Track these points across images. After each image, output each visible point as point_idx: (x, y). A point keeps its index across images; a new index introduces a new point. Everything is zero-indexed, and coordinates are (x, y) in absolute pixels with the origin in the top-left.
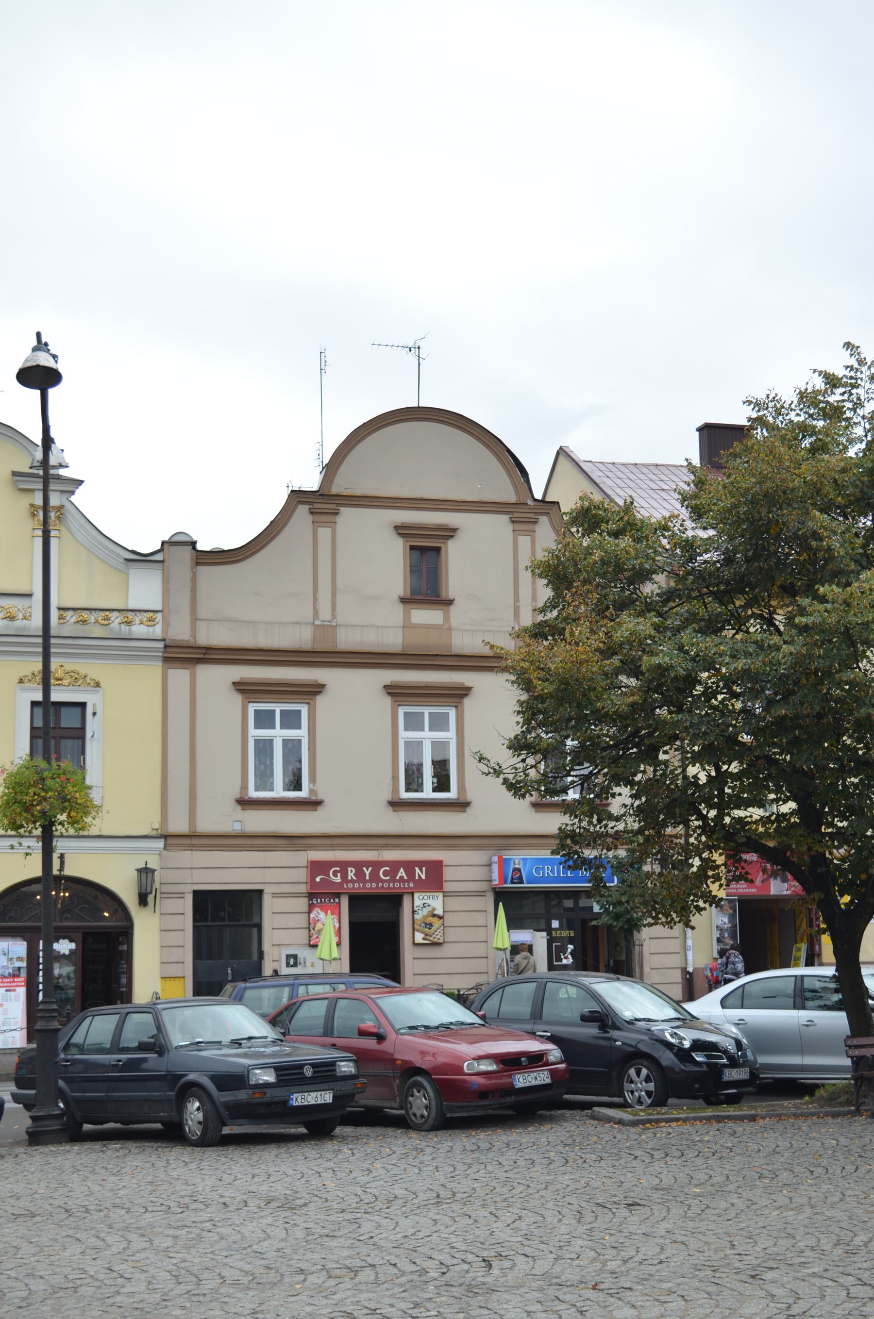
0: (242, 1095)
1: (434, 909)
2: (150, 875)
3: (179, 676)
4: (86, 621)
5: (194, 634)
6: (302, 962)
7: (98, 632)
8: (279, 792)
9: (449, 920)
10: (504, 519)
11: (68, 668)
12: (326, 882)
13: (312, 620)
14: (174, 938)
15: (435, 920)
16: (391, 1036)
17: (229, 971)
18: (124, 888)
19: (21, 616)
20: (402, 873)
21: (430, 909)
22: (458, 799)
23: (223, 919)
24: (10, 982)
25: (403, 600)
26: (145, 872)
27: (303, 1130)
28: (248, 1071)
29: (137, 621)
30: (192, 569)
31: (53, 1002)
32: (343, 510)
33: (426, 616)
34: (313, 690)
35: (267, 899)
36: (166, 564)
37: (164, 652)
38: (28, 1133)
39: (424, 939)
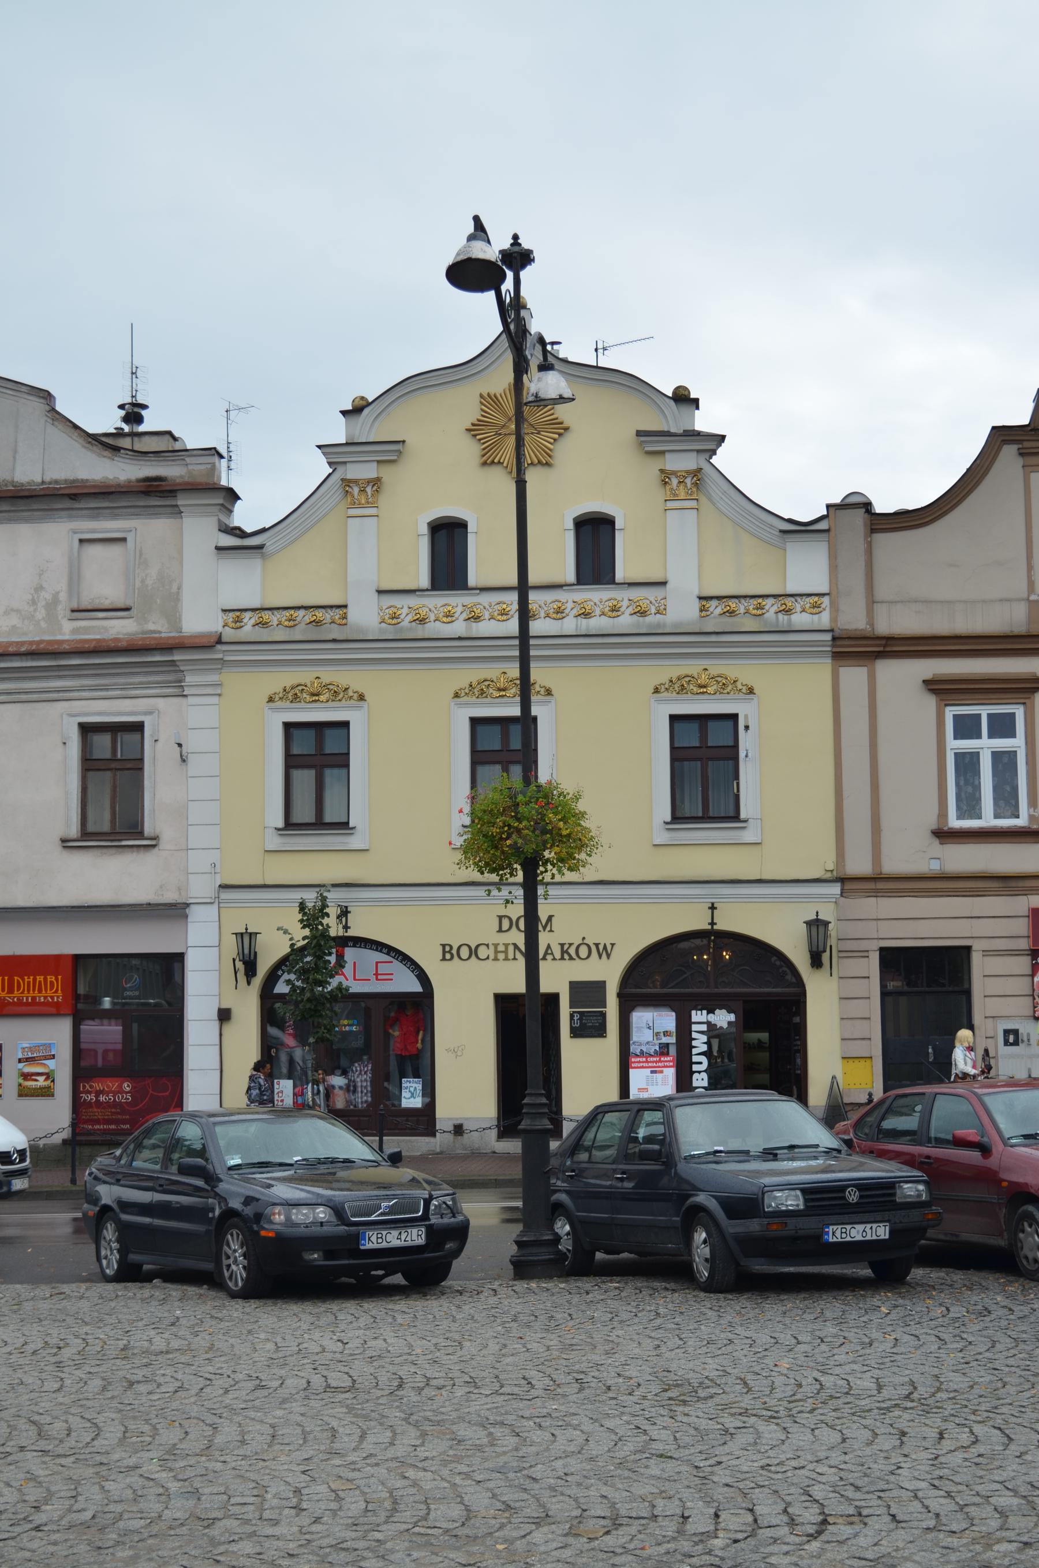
0: (754, 1226)
2: (821, 929)
3: (854, 675)
4: (734, 611)
5: (871, 621)
6: (1025, 1039)
7: (750, 624)
8: (988, 820)
11: (714, 671)
13: (1025, 595)
14: (857, 1009)
16: (998, 1148)
17: (930, 1050)
18: (793, 945)
19: (653, 611)
23: (944, 985)
24: (656, 1062)
26: (817, 926)
27: (867, 1272)
28: (763, 1194)
30: (866, 538)
31: (541, 1095)
35: (976, 958)
36: (832, 533)
37: (833, 646)
38: (512, 1262)
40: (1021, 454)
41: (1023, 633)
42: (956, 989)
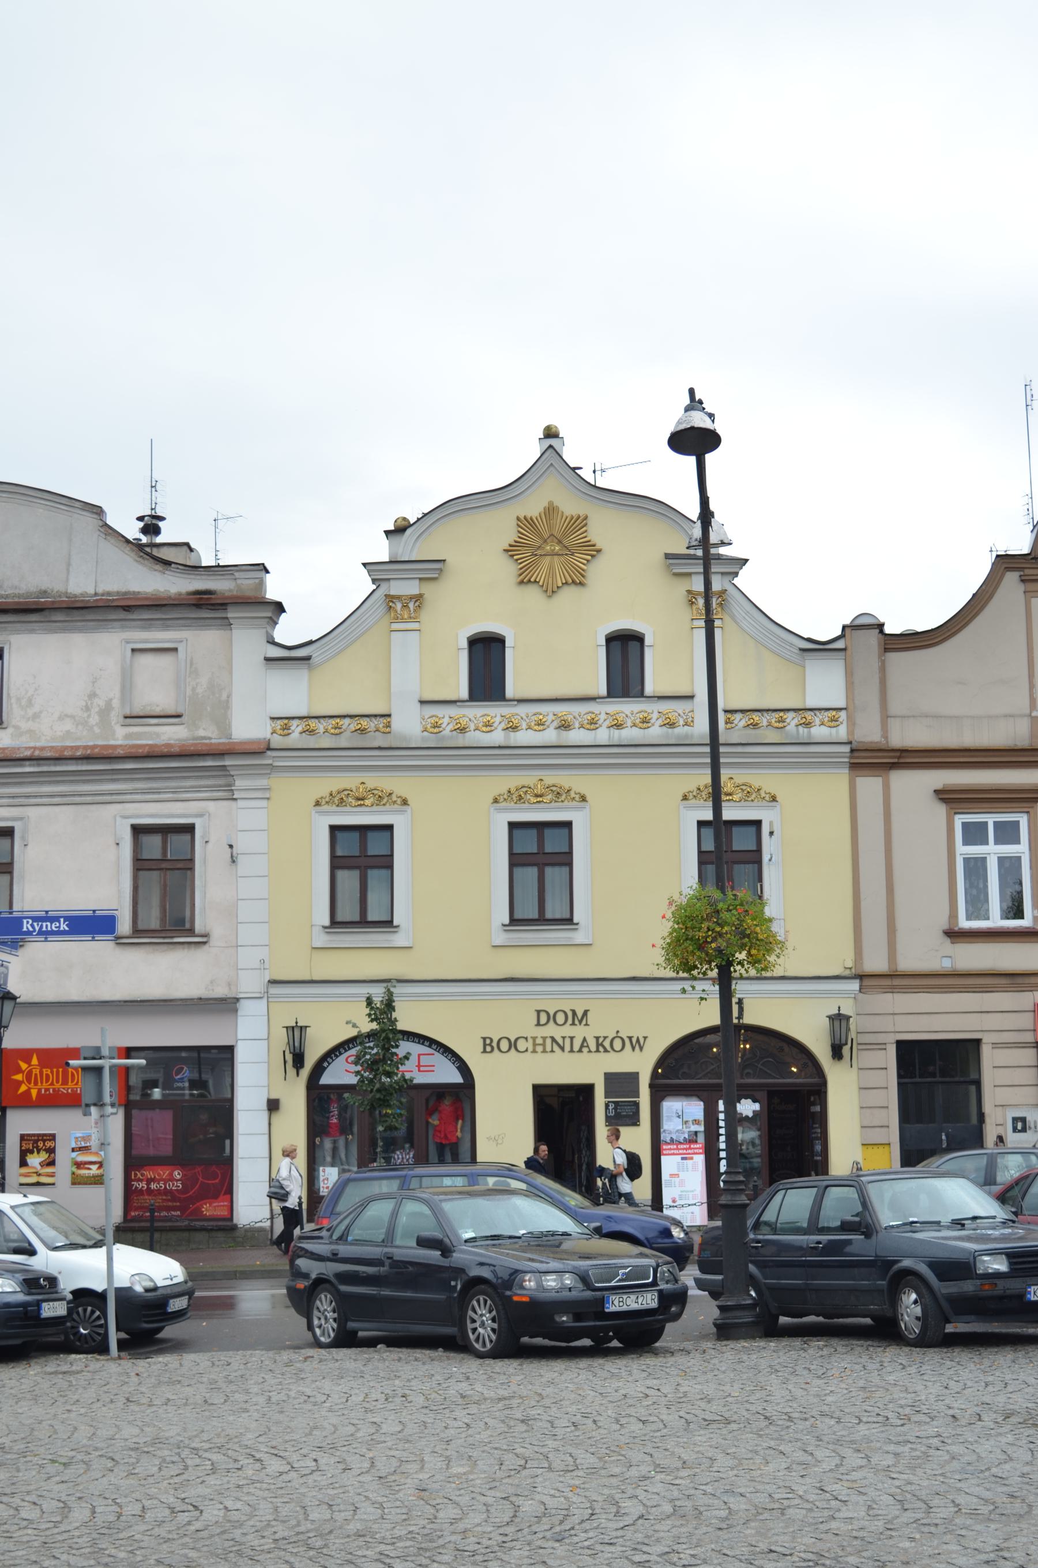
3: (870, 785)
6: (1032, 1126)
8: (996, 920)
13: (1028, 712)
17: (944, 1137)
29: (817, 722)
40: (1022, 581)
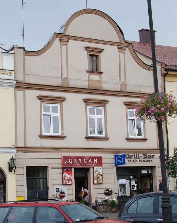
1: (100, 173)
2: (14, 161)
3: (20, 93)
8: (52, 134)
9: (104, 176)
10: (116, 47)
12: (68, 163)
13: (61, 77)
15: (100, 176)
17: (37, 194)
20: (90, 161)
21: (99, 172)
22: (105, 137)
25: (88, 72)
29: (6, 73)
32: (70, 41)
33: (95, 77)
34: (63, 100)
39: (97, 182)
40: (60, 41)
41: (87, 88)
42: (38, 177)
